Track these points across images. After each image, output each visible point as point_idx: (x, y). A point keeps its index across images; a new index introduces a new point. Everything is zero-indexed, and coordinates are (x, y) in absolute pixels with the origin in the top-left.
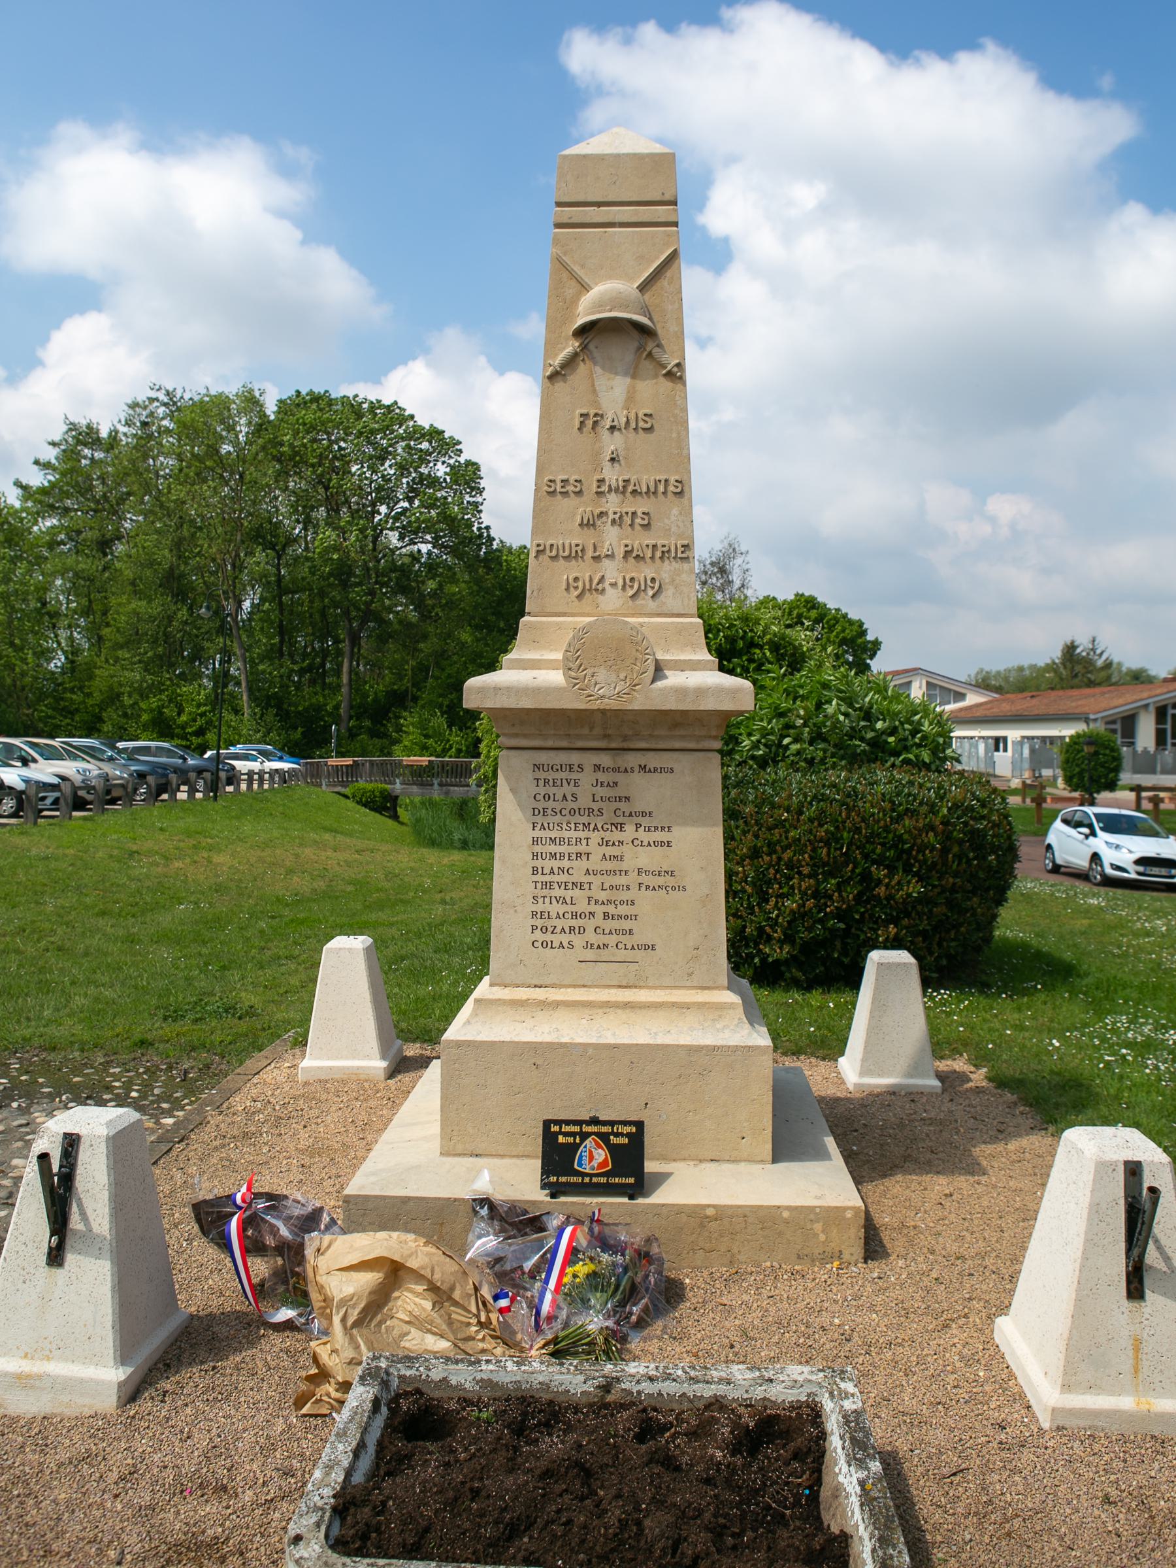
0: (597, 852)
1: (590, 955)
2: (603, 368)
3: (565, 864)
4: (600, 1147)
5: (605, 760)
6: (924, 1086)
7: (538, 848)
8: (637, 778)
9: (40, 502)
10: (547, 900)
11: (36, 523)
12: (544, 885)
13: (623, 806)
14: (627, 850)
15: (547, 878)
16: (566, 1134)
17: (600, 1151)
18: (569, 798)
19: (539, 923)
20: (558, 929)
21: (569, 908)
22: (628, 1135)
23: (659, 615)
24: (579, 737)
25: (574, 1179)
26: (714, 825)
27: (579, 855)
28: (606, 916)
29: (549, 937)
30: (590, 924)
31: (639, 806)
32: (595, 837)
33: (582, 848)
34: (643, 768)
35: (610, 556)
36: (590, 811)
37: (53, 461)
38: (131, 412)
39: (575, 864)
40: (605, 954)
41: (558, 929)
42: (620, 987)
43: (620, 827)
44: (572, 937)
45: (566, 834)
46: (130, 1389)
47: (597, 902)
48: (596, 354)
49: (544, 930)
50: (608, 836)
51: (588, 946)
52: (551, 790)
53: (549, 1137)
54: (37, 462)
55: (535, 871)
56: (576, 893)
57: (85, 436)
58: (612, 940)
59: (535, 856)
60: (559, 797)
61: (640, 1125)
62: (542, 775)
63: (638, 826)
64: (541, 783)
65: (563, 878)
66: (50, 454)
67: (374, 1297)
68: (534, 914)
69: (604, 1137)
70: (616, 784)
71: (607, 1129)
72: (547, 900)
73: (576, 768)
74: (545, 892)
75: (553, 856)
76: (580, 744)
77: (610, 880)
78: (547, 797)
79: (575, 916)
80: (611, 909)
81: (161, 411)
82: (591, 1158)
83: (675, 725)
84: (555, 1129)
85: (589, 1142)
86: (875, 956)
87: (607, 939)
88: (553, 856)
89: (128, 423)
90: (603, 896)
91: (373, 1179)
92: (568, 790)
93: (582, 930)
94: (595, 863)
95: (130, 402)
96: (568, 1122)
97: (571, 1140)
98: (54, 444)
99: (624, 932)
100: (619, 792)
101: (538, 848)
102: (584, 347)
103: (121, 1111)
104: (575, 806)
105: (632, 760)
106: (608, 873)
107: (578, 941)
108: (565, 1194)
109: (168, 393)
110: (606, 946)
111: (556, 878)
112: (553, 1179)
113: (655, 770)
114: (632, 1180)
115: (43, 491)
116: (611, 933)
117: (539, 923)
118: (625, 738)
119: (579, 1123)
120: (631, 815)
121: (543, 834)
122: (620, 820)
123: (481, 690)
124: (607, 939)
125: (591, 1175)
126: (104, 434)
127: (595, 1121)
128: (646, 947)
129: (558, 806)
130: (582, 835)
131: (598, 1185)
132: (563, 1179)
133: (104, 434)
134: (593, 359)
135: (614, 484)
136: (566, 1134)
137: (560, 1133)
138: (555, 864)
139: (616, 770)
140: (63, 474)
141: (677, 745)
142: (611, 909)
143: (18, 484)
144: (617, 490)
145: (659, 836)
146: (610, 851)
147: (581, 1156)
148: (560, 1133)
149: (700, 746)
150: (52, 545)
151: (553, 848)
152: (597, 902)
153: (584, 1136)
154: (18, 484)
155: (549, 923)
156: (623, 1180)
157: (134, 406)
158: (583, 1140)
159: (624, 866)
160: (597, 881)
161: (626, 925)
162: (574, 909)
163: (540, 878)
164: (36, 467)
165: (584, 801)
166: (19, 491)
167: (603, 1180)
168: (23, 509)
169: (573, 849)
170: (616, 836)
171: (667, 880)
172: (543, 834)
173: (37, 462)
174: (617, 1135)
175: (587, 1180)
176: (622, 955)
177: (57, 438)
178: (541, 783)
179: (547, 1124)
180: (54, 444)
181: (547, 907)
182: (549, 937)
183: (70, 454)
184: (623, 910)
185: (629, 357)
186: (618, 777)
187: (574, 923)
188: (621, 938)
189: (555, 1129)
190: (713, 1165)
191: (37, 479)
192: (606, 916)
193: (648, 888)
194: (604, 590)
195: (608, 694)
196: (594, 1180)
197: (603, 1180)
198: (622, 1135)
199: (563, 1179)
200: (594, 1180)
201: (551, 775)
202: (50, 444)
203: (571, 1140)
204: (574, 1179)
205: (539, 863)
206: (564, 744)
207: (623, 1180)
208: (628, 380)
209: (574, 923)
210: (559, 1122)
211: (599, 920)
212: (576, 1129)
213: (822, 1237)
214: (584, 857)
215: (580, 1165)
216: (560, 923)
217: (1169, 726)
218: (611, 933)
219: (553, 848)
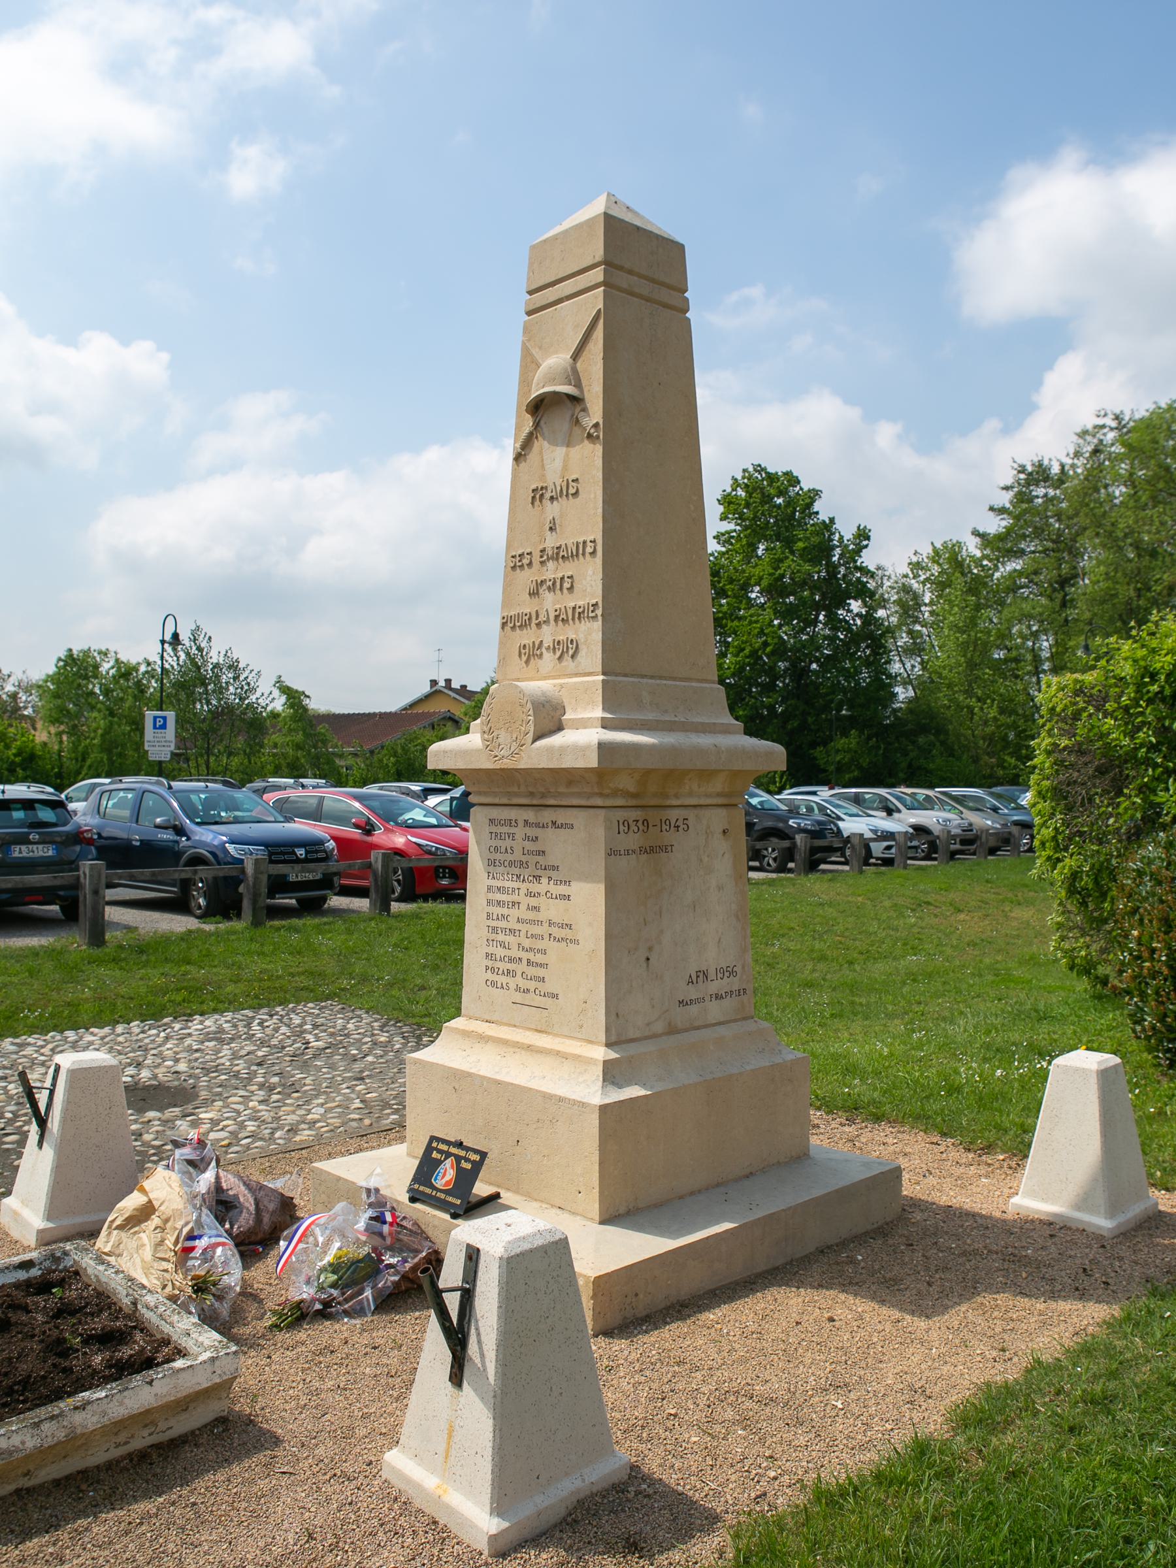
1: (518, 997)
2: (549, 443)
3: (505, 911)
6: (1089, 1224)
8: (550, 831)
9: (999, 550)
11: (996, 569)
14: (541, 901)
22: (473, 1162)
23: (577, 675)
24: (516, 795)
25: (428, 1191)
26: (599, 882)
31: (551, 860)
32: (524, 887)
33: (515, 898)
35: (547, 622)
37: (1008, 505)
38: (1081, 441)
42: (537, 1030)
43: (537, 878)
46: (48, 1238)
48: (545, 430)
51: (518, 989)
53: (429, 1149)
54: (992, 509)
56: (509, 939)
57: (1039, 474)
61: (484, 1155)
62: (494, 829)
63: (550, 878)
66: (1005, 499)
67: (135, 1213)
69: (458, 1159)
78: (496, 849)
79: (511, 960)
81: (1111, 436)
83: (570, 783)
84: (434, 1144)
89: (1077, 454)
95: (1079, 430)
97: (439, 1156)
98: (1006, 488)
102: (537, 425)
103: (108, 1056)
105: (547, 816)
108: (423, 1202)
109: (1117, 418)
112: (416, 1186)
115: (1001, 538)
117: (490, 964)
118: (543, 796)
119: (448, 1143)
122: (539, 873)
123: (437, 754)
126: (1056, 469)
127: (460, 1145)
131: (438, 1199)
132: (422, 1188)
133: (1056, 469)
134: (543, 435)
135: (550, 553)
136: (440, 1151)
139: (537, 825)
140: (1017, 518)
141: (575, 802)
142: (531, 956)
143: (975, 533)
144: (552, 558)
145: (562, 889)
149: (589, 804)
150: (1014, 589)
153: (448, 1155)
154: (975, 533)
157: (1083, 434)
161: (540, 972)
164: (991, 514)
165: (518, 855)
166: (978, 540)
167: (443, 1196)
168: (984, 557)
171: (564, 932)
173: (992, 509)
174: (467, 1160)
177: (1009, 482)
179: (433, 1138)
180: (1006, 488)
183: (1023, 497)
184: (539, 958)
185: (566, 426)
190: (559, 1211)
191: (995, 525)
194: (541, 654)
195: (506, 754)
197: (443, 1196)
199: (422, 1188)
200: (439, 1194)
202: (1003, 489)
203: (439, 1156)
204: (428, 1191)
206: (505, 801)
208: (564, 449)
210: (439, 1140)
212: (444, 1147)
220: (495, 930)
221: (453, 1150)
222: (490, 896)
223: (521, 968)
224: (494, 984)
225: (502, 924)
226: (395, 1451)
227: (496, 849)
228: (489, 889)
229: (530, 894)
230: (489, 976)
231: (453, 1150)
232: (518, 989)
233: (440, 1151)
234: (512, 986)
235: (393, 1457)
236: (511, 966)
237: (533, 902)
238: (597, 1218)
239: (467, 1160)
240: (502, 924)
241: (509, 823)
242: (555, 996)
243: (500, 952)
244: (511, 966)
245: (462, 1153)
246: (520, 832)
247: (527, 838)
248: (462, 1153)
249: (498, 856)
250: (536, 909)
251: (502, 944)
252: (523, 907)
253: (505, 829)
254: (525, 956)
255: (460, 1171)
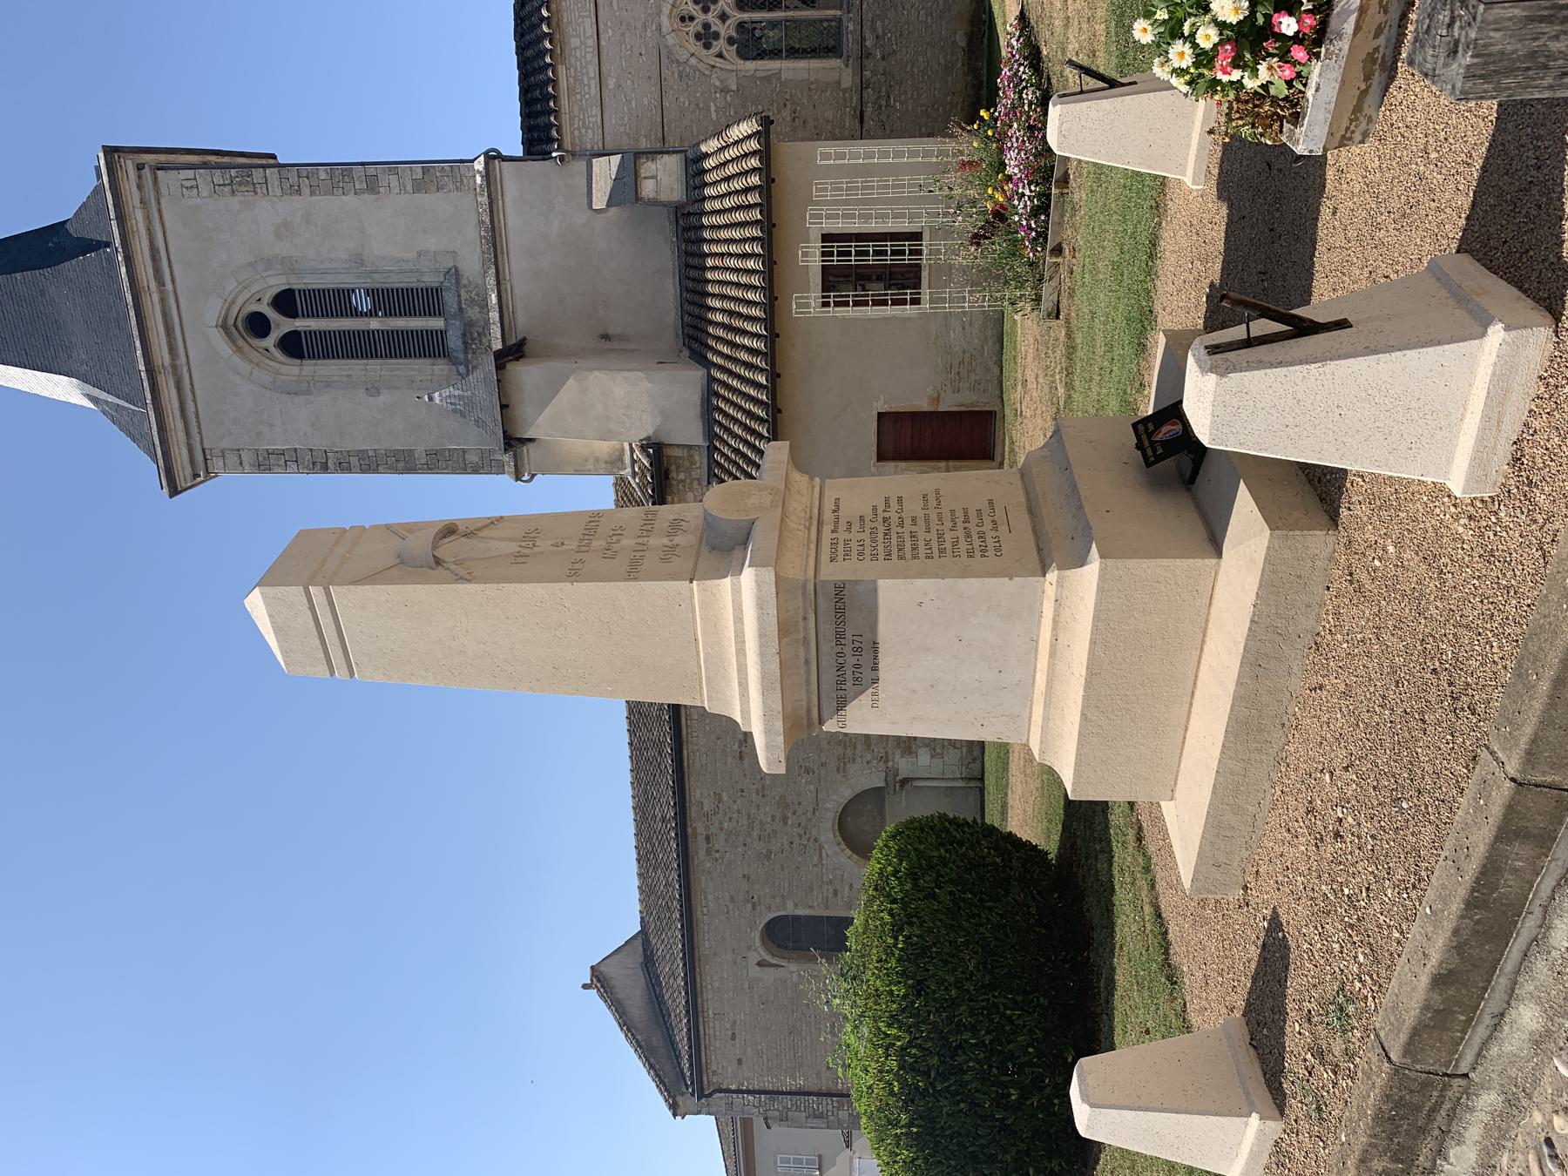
1: (1003, 529)
56: (948, 537)
78: (861, 554)
117: (978, 554)
136: (1154, 451)
139: (836, 523)
220: (942, 551)
221: (1146, 443)
222: (908, 556)
223: (972, 526)
224: (998, 549)
225: (935, 545)
226: (1449, 484)
227: (861, 554)
228: (901, 558)
229: (901, 525)
230: (991, 552)
231: (1146, 443)
233: (1154, 451)
234: (994, 534)
235: (1457, 486)
236: (975, 537)
237: (908, 522)
238: (1214, 561)
240: (935, 545)
241: (834, 544)
242: (991, 502)
243: (963, 545)
244: (975, 537)
245: (1144, 437)
246: (842, 536)
247: (849, 530)
248: (1144, 437)
249: (868, 551)
250: (914, 519)
251: (955, 543)
252: (914, 529)
253: (841, 547)
254: (960, 526)
255: (1157, 427)
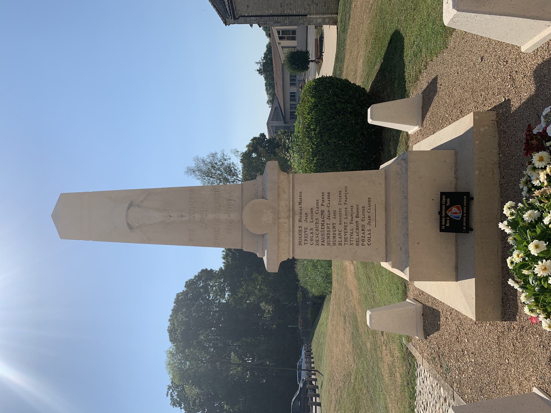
0: (332, 220)
1: (373, 223)
3: (337, 232)
4: (451, 210)
5: (297, 218)
7: (331, 243)
10: (352, 239)
12: (346, 241)
13: (314, 211)
15: (343, 239)
16: (446, 223)
17: (453, 209)
18: (312, 231)
19: (361, 242)
20: (363, 235)
21: (355, 231)
22: (446, 198)
25: (465, 218)
27: (334, 227)
28: (357, 217)
29: (366, 239)
30: (361, 223)
31: (315, 205)
32: (327, 221)
33: (331, 226)
34: (300, 203)
36: (316, 223)
39: (337, 229)
40: (373, 217)
41: (363, 235)
44: (366, 230)
45: (326, 232)
47: (352, 220)
49: (363, 241)
50: (326, 217)
51: (369, 224)
52: (309, 238)
55: (340, 244)
56: (349, 228)
58: (367, 215)
59: (334, 244)
60: (311, 235)
62: (303, 242)
64: (306, 242)
65: (343, 233)
68: (357, 245)
69: (447, 208)
70: (306, 214)
71: (444, 207)
72: (352, 239)
73: (300, 229)
74: (348, 240)
75: (334, 237)
76: (291, 227)
77: (344, 216)
78: (312, 240)
79: (357, 229)
80: (354, 215)
82: (456, 213)
84: (443, 227)
85: (449, 214)
86: (370, 121)
87: (366, 217)
88: (334, 237)
90: (349, 218)
91: (468, 308)
92: (309, 232)
93: (363, 226)
94: (337, 221)
96: (441, 222)
97: (448, 221)
99: (364, 210)
100: (309, 212)
101: (331, 243)
104: (315, 229)
106: (340, 216)
107: (367, 227)
110: (369, 217)
111: (343, 236)
112: (464, 228)
113: (300, 199)
114: (465, 197)
116: (364, 215)
117: (361, 242)
120: (318, 208)
121: (326, 241)
122: (320, 211)
124: (366, 217)
125: (463, 213)
128: (369, 201)
129: (315, 236)
130: (326, 227)
132: (465, 224)
136: (446, 223)
137: (445, 225)
138: (337, 236)
139: (301, 213)
146: (332, 215)
147: (455, 217)
148: (445, 225)
149: (292, 182)
151: (331, 237)
152: (352, 220)
153: (447, 216)
155: (361, 239)
156: (465, 200)
158: (449, 216)
159: (338, 210)
160: (344, 220)
161: (361, 209)
162: (355, 229)
163: (343, 243)
167: (465, 208)
169: (331, 230)
170: (326, 213)
172: (326, 241)
174: (446, 202)
175: (465, 215)
176: (372, 211)
178: (306, 242)
179: (441, 230)
181: (354, 239)
182: (366, 239)
184: (355, 210)
186: (303, 213)
187: (360, 229)
188: (366, 211)
189: (443, 227)
192: (357, 217)
193: (346, 201)
196: (465, 212)
197: (465, 208)
198: (446, 201)
199: (465, 224)
200: (465, 212)
201: (303, 238)
203: (448, 221)
205: (337, 243)
207: (465, 200)
209: (360, 229)
210: (441, 226)
211: (359, 220)
212: (444, 219)
213: (486, 128)
214: (335, 225)
215: (459, 217)
216: (361, 235)
217: (286, 36)
218: (364, 215)
219: (331, 237)
224: (369, 240)
227: (312, 240)
232: (369, 224)
235: (523, 50)
239: (446, 202)
